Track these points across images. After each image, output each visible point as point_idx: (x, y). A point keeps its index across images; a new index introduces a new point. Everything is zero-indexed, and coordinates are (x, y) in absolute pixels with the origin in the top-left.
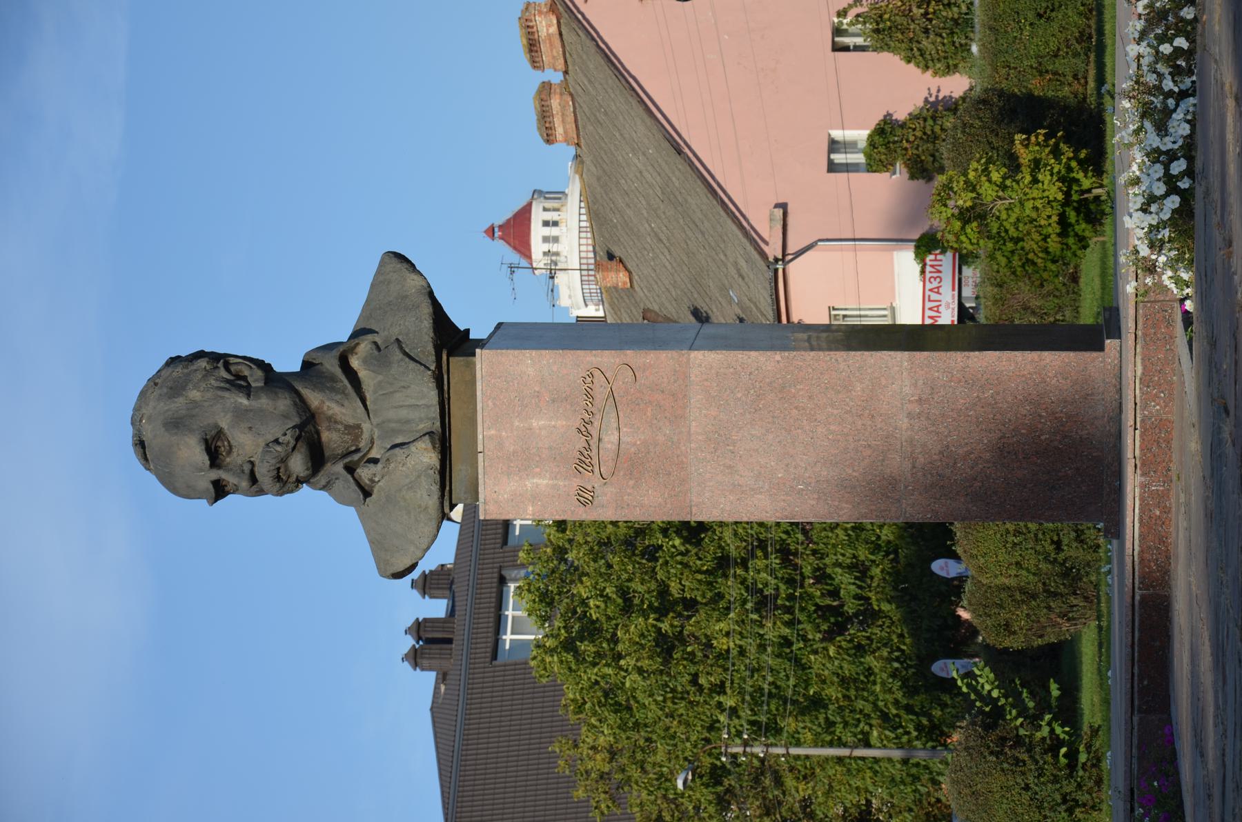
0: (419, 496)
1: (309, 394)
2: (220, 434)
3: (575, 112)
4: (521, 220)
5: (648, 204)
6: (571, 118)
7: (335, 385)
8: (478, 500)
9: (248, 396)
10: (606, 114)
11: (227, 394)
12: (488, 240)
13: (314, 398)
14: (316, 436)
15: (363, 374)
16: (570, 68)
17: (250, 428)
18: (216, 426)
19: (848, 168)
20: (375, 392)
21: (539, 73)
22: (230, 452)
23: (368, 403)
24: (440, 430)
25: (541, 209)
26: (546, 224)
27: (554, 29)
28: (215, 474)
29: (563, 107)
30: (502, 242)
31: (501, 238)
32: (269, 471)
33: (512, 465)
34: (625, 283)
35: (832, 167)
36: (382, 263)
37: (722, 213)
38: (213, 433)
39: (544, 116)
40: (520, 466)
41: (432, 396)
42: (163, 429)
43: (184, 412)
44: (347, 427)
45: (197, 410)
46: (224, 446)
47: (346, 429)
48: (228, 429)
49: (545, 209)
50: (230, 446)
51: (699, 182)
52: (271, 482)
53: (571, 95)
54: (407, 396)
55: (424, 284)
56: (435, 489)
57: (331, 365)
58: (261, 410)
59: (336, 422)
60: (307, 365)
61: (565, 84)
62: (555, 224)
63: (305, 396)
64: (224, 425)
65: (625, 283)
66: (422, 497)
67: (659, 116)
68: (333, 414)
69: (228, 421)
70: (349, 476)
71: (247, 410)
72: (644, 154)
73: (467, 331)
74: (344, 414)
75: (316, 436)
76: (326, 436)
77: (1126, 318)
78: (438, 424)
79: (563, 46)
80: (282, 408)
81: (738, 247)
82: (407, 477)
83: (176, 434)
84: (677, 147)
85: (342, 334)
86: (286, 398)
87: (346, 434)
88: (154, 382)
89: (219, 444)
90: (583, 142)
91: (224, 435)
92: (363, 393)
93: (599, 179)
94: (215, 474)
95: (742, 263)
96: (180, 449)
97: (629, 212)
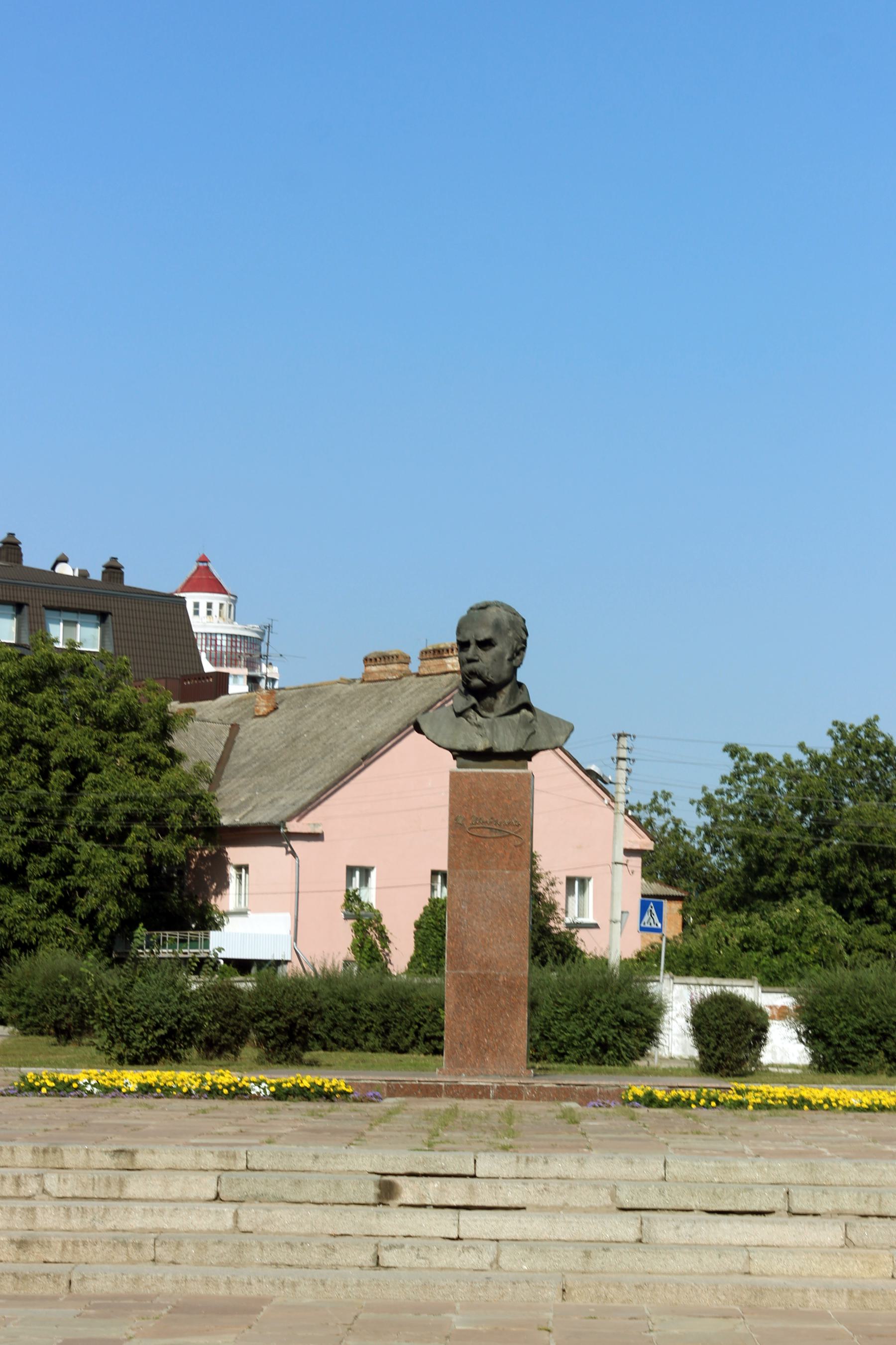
3: (388, 680)
4: (215, 586)
5: (322, 733)
6: (383, 676)
10: (389, 704)
12: (197, 557)
13: (506, 690)
16: (421, 679)
19: (349, 882)
21: (418, 655)
25: (222, 602)
26: (209, 605)
27: (450, 668)
29: (392, 672)
30: (195, 567)
31: (198, 568)
34: (258, 711)
35: (351, 870)
36: (569, 724)
37: (319, 790)
39: (384, 658)
49: (221, 605)
51: (343, 772)
53: (401, 678)
57: (520, 700)
60: (520, 685)
61: (408, 674)
62: (209, 613)
65: (258, 711)
67: (389, 744)
70: (469, 705)
72: (360, 731)
77: (726, 1082)
79: (438, 674)
81: (290, 799)
84: (368, 757)
85: (535, 703)
88: (515, 614)
90: (365, 685)
93: (338, 696)
94: (472, 642)
95: (282, 802)
97: (314, 718)
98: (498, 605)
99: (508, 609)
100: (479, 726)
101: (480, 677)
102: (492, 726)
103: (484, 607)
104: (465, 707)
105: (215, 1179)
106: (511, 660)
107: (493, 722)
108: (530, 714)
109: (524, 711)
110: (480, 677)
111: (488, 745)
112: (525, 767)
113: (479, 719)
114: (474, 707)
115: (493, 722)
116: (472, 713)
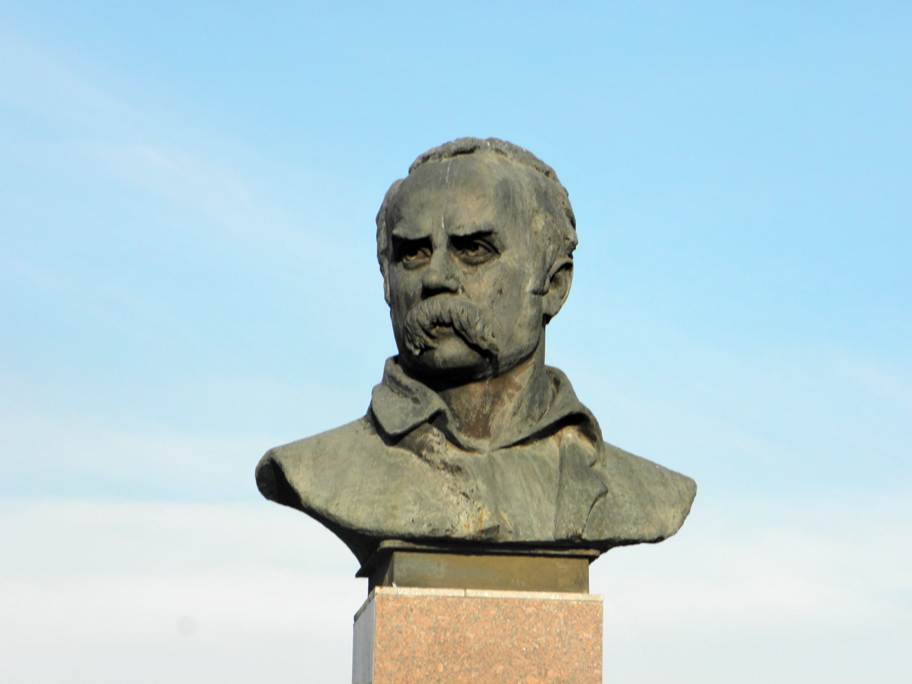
0: (410, 507)
1: (527, 370)
2: (494, 251)
7: (537, 405)
8: (400, 585)
9: (535, 292)
11: (538, 264)
14: (480, 376)
15: (552, 442)
17: (500, 292)
18: (504, 248)
20: (534, 457)
22: (469, 263)
23: (518, 448)
24: (501, 541)
28: (440, 240)
32: (450, 312)
33: (448, 634)
36: (686, 479)
38: (497, 244)
40: (446, 644)
41: (548, 535)
42: (501, 179)
43: (520, 207)
44: (487, 418)
45: (522, 224)
46: (477, 255)
47: (484, 416)
48: (500, 263)
50: (476, 264)
52: (433, 313)
54: (539, 499)
55: (670, 530)
56: (424, 530)
58: (519, 307)
59: (493, 404)
63: (524, 365)
64: (504, 257)
66: (408, 511)
68: (503, 401)
69: (509, 264)
70: (426, 415)
71: (520, 288)
73: (359, 574)
74: (503, 415)
75: (480, 376)
76: (476, 390)
78: (511, 538)
80: (520, 335)
82: (434, 493)
83: (497, 195)
86: (529, 340)
87: (478, 416)
89: (481, 250)
91: (491, 257)
92: (532, 443)
94: (440, 240)
96: (478, 198)
98: (499, 147)
99: (527, 158)
100: (455, 469)
101: (461, 334)
102: (490, 473)
103: (467, 150)
104: (412, 421)
105: (593, 467)
106: (539, 292)
107: (492, 461)
108: (585, 444)
109: (570, 434)
110: (461, 334)
111: (487, 520)
112: (581, 584)
113: (452, 454)
114: (437, 419)
115: (492, 461)
116: (434, 436)
